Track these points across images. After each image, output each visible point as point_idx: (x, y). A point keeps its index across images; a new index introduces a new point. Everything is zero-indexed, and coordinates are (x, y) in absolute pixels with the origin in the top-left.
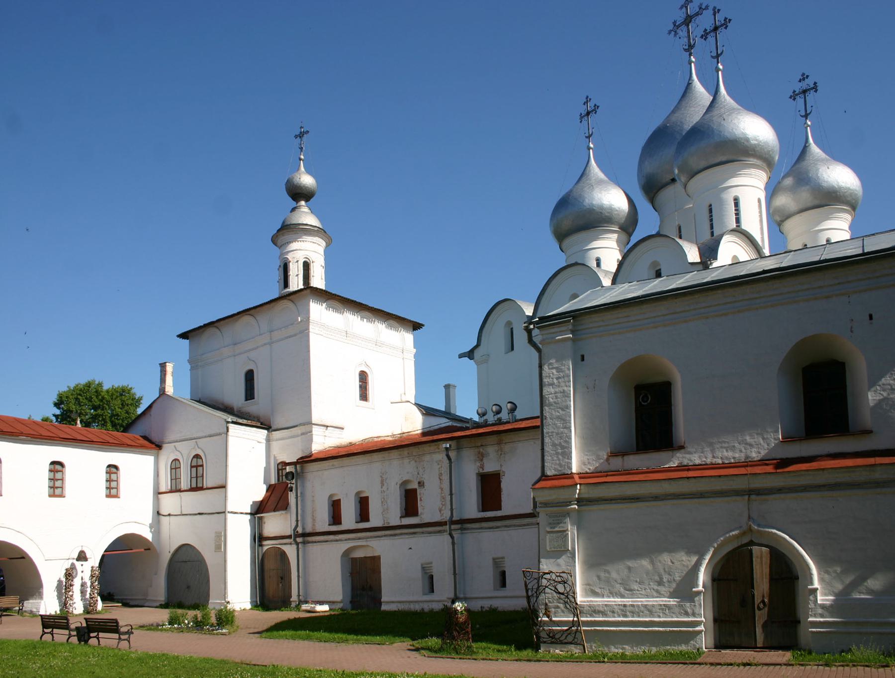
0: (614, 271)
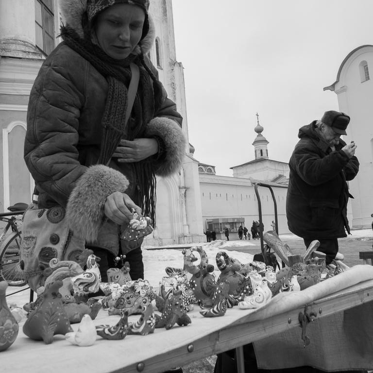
0: (269, 159)
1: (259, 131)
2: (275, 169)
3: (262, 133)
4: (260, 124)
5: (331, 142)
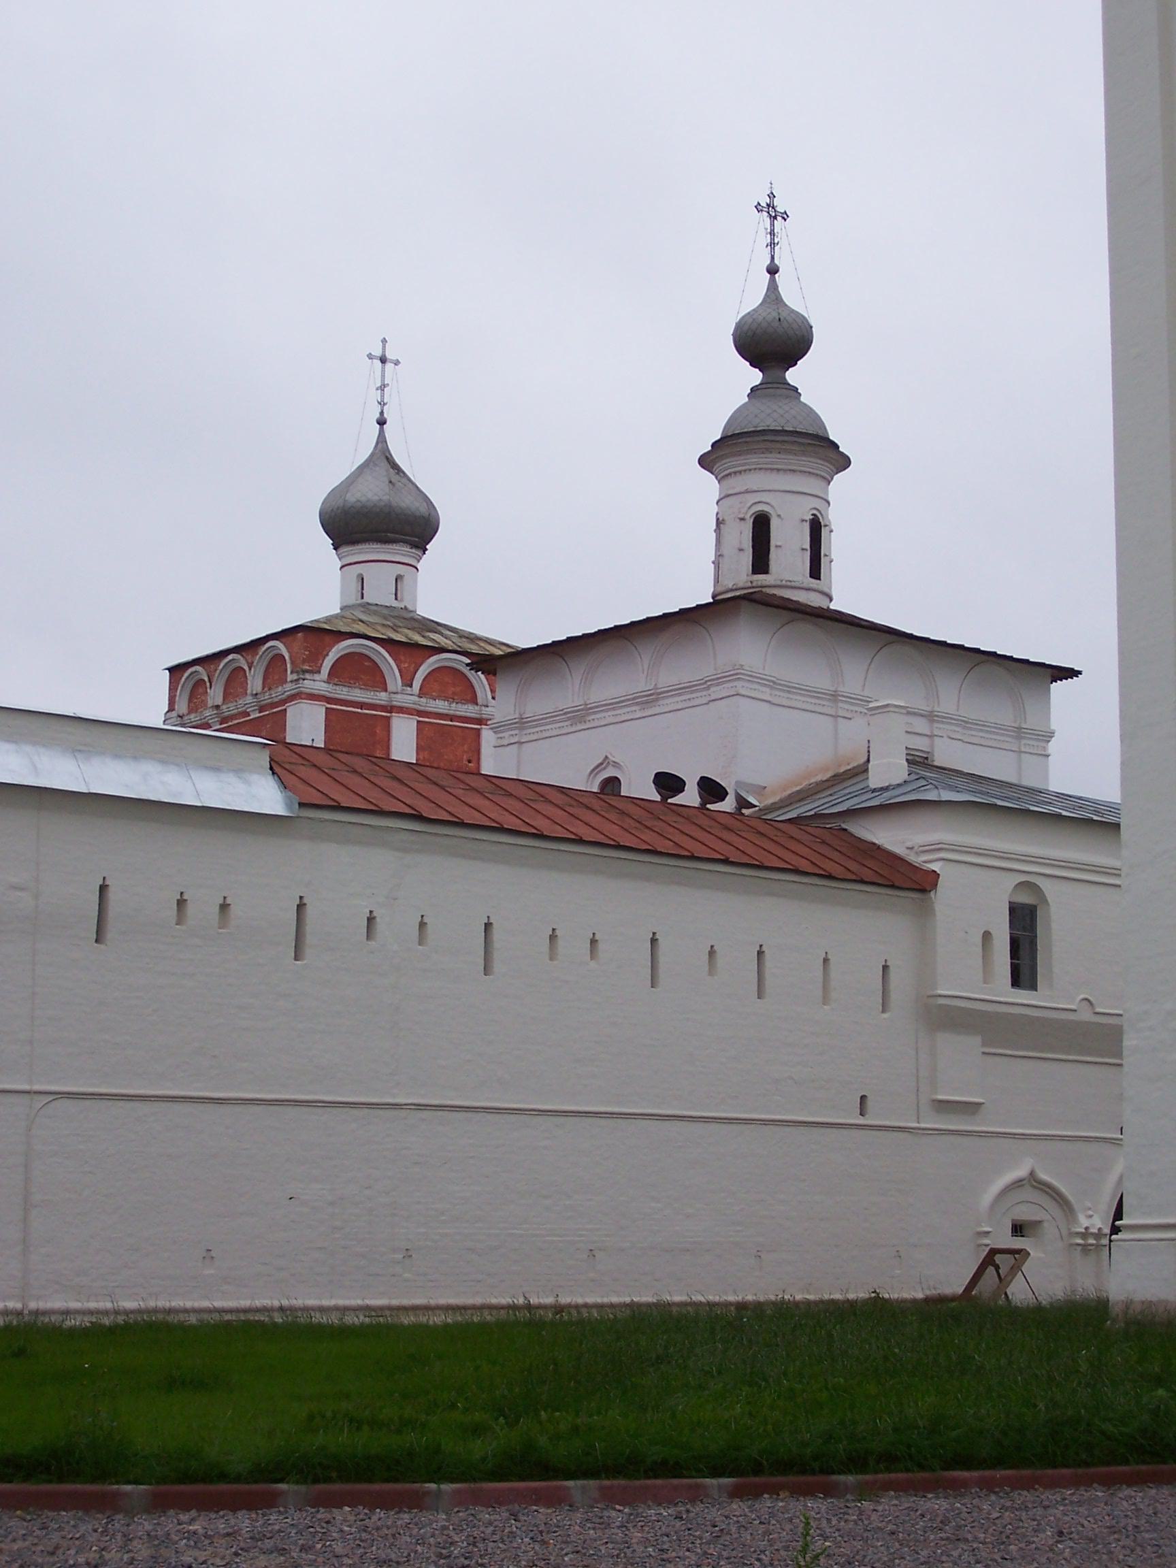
1: (773, 345)
2: (834, 697)
3: (793, 376)
4: (776, 261)
5: (1084, 1367)
